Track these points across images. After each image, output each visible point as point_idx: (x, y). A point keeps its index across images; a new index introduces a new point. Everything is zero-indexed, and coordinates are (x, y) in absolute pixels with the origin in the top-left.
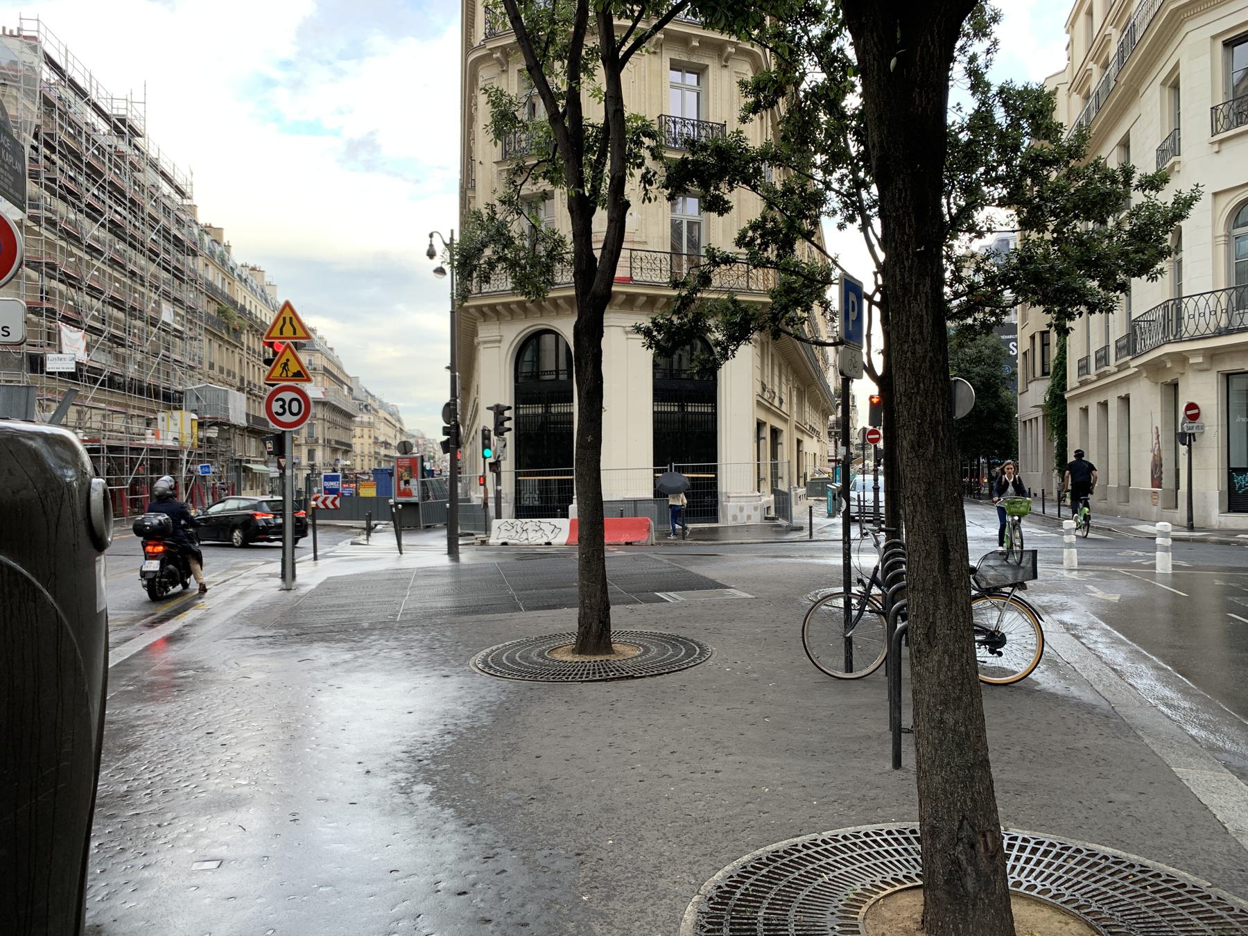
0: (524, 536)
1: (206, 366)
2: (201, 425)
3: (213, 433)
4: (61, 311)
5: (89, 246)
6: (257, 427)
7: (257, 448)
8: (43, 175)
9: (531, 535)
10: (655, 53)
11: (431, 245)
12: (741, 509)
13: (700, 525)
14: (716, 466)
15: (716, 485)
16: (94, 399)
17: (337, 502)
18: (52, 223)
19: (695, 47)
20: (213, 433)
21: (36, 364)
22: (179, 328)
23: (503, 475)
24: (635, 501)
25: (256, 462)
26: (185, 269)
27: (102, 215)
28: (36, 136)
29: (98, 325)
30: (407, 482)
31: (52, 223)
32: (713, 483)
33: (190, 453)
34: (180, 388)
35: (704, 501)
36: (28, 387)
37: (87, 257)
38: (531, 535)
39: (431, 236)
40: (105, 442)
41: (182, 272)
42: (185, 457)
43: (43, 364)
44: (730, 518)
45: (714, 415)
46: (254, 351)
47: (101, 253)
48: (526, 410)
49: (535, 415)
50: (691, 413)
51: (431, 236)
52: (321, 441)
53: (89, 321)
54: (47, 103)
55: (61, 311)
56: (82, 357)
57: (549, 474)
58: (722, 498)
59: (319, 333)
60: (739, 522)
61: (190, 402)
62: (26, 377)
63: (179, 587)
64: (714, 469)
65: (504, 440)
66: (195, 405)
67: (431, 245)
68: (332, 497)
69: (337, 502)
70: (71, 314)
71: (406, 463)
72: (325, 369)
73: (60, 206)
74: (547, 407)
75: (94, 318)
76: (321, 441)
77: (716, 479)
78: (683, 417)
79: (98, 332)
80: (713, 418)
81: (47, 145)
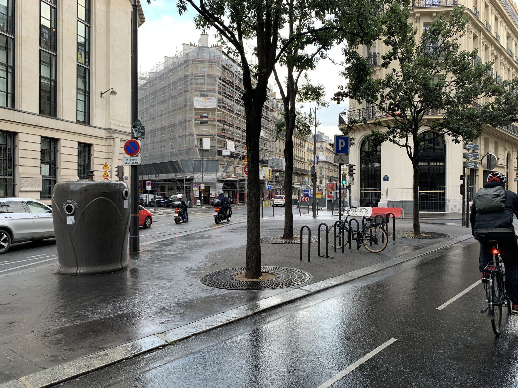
0: (356, 213)
1: (278, 150)
2: (273, 171)
3: (277, 174)
4: (227, 135)
5: (236, 113)
6: (297, 172)
7: (298, 179)
8: (222, 92)
9: (358, 213)
10: (416, 22)
11: (311, 113)
12: (455, 206)
13: (430, 212)
14: (445, 188)
15: (445, 195)
16: (237, 164)
17: (309, 199)
18: (224, 107)
19: (435, 16)
20: (277, 174)
21: (220, 153)
22: (267, 138)
23: (352, 191)
24: (402, 202)
25: (297, 185)
26: (269, 117)
27: (240, 102)
28: (220, 79)
29: (239, 139)
30: (331, 193)
31: (224, 107)
32: (444, 195)
33: (269, 182)
34: (267, 159)
35: (438, 203)
36: (217, 161)
37: (236, 116)
38: (358, 213)
39: (311, 109)
40: (239, 178)
41: (268, 118)
42: (267, 183)
43: (222, 153)
44: (449, 210)
45: (444, 166)
46: (297, 144)
47: (240, 115)
48: (365, 166)
49: (368, 168)
50: (433, 166)
51: (311, 109)
52: (324, 177)
53: (236, 138)
54: (223, 67)
55: (227, 135)
56: (233, 150)
57: (372, 190)
58: (447, 201)
59: (325, 135)
60: (455, 211)
61: (270, 164)
62: (217, 158)
63: (226, 221)
64: (444, 189)
65: (353, 177)
66: (271, 165)
67: (311, 113)
68: (307, 197)
69: (309, 199)
70: (230, 137)
71: (331, 185)
72: (327, 148)
73: (227, 100)
74: (372, 164)
75: (238, 137)
76: (324, 177)
77: (445, 193)
78: (429, 169)
79: (239, 141)
80: (444, 168)
81: (223, 81)
